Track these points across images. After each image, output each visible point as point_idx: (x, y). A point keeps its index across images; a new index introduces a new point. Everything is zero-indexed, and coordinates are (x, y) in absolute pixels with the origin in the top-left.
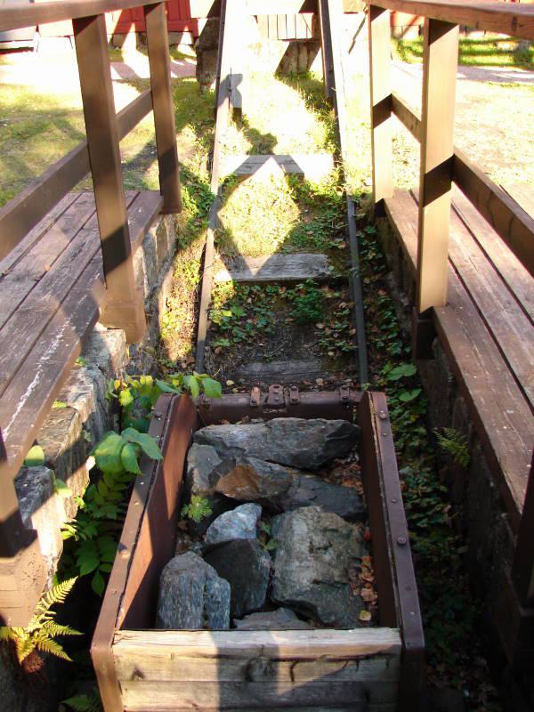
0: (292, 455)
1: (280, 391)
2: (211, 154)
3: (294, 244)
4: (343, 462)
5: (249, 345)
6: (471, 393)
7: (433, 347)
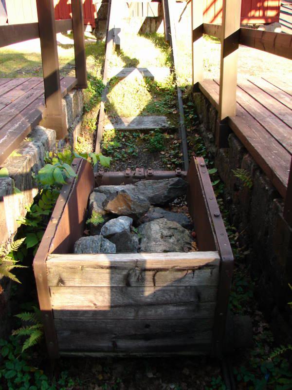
0: (149, 197)
1: (142, 170)
2: (103, 66)
3: (148, 112)
4: (178, 206)
5: (123, 161)
6: (253, 145)
7: (228, 139)
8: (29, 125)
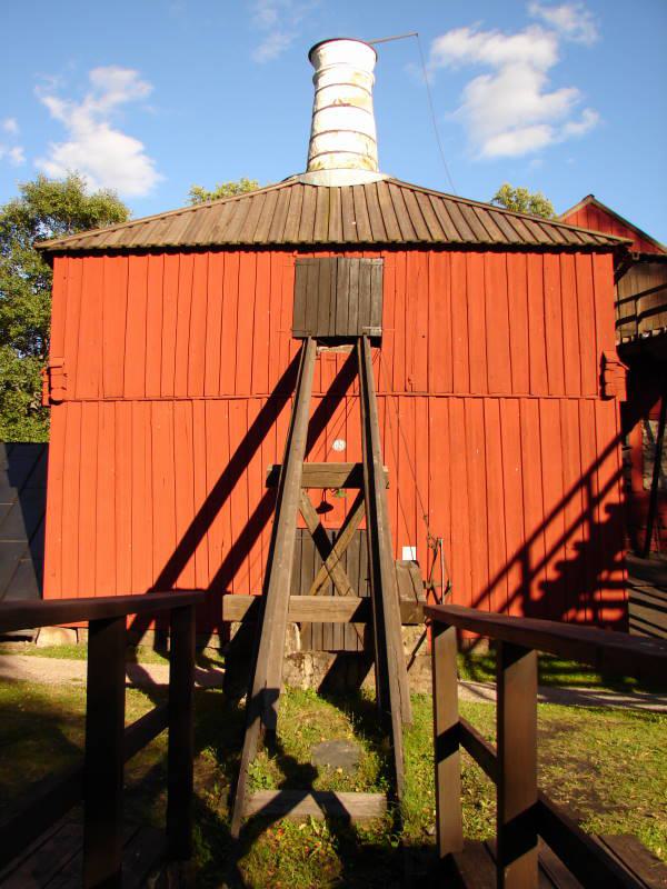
8: (351, 735)
